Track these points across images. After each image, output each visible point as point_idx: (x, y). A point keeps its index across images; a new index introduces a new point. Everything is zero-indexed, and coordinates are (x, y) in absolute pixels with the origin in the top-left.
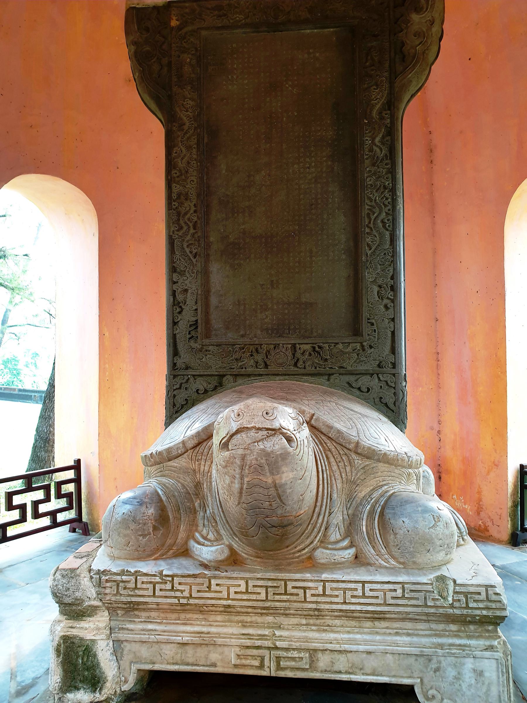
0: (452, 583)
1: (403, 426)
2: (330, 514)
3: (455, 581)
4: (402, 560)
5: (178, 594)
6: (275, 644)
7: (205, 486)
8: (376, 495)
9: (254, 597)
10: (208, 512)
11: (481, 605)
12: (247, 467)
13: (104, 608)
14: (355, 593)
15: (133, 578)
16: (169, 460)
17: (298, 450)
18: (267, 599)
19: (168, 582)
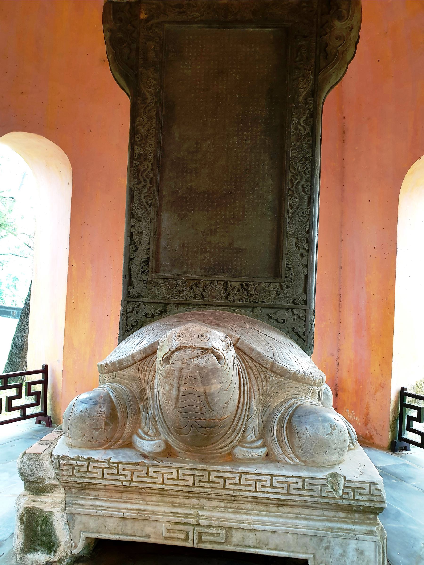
0: (343, 480)
1: (310, 351)
2: (248, 419)
3: (345, 478)
4: (304, 459)
5: (122, 478)
6: (198, 522)
7: (148, 392)
8: (285, 406)
9: (183, 483)
10: (150, 413)
11: (365, 498)
12: (184, 378)
13: (61, 487)
14: (265, 484)
15: (86, 463)
16: (121, 370)
17: (226, 366)
19: (114, 468)
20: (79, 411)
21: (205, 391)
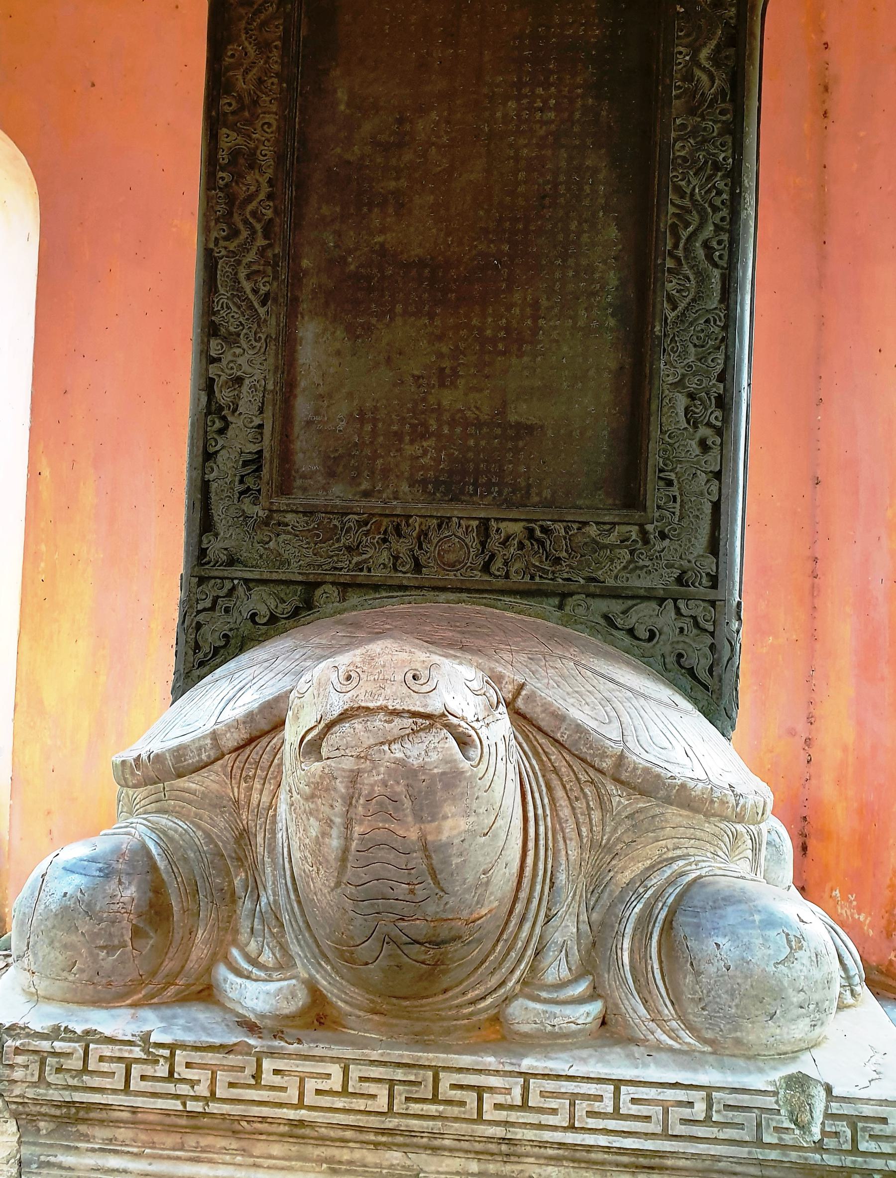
1: (728, 723)
3: (829, 1089)
4: (709, 1035)
7: (260, 839)
8: (656, 880)
9: (360, 1104)
10: (264, 900)
14: (597, 1106)
16: (180, 776)
19: (162, 1061)
20: (58, 895)
21: (423, 838)
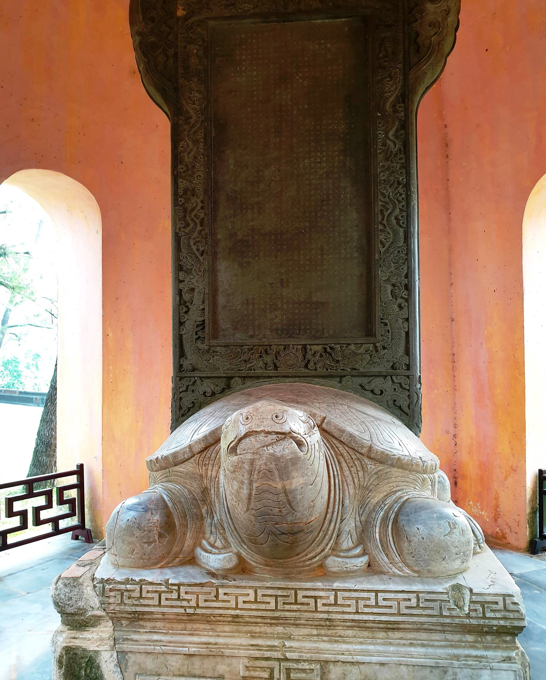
0: (469, 593)
1: (418, 430)
2: (342, 520)
3: (471, 590)
4: (416, 569)
5: (185, 603)
6: (285, 656)
7: (212, 492)
8: (389, 501)
9: (263, 607)
10: (215, 518)
11: (498, 615)
12: (256, 472)
13: (108, 618)
14: (368, 603)
15: (137, 587)
17: (309, 454)
18: (276, 609)
19: (174, 591)
21: (284, 487)
